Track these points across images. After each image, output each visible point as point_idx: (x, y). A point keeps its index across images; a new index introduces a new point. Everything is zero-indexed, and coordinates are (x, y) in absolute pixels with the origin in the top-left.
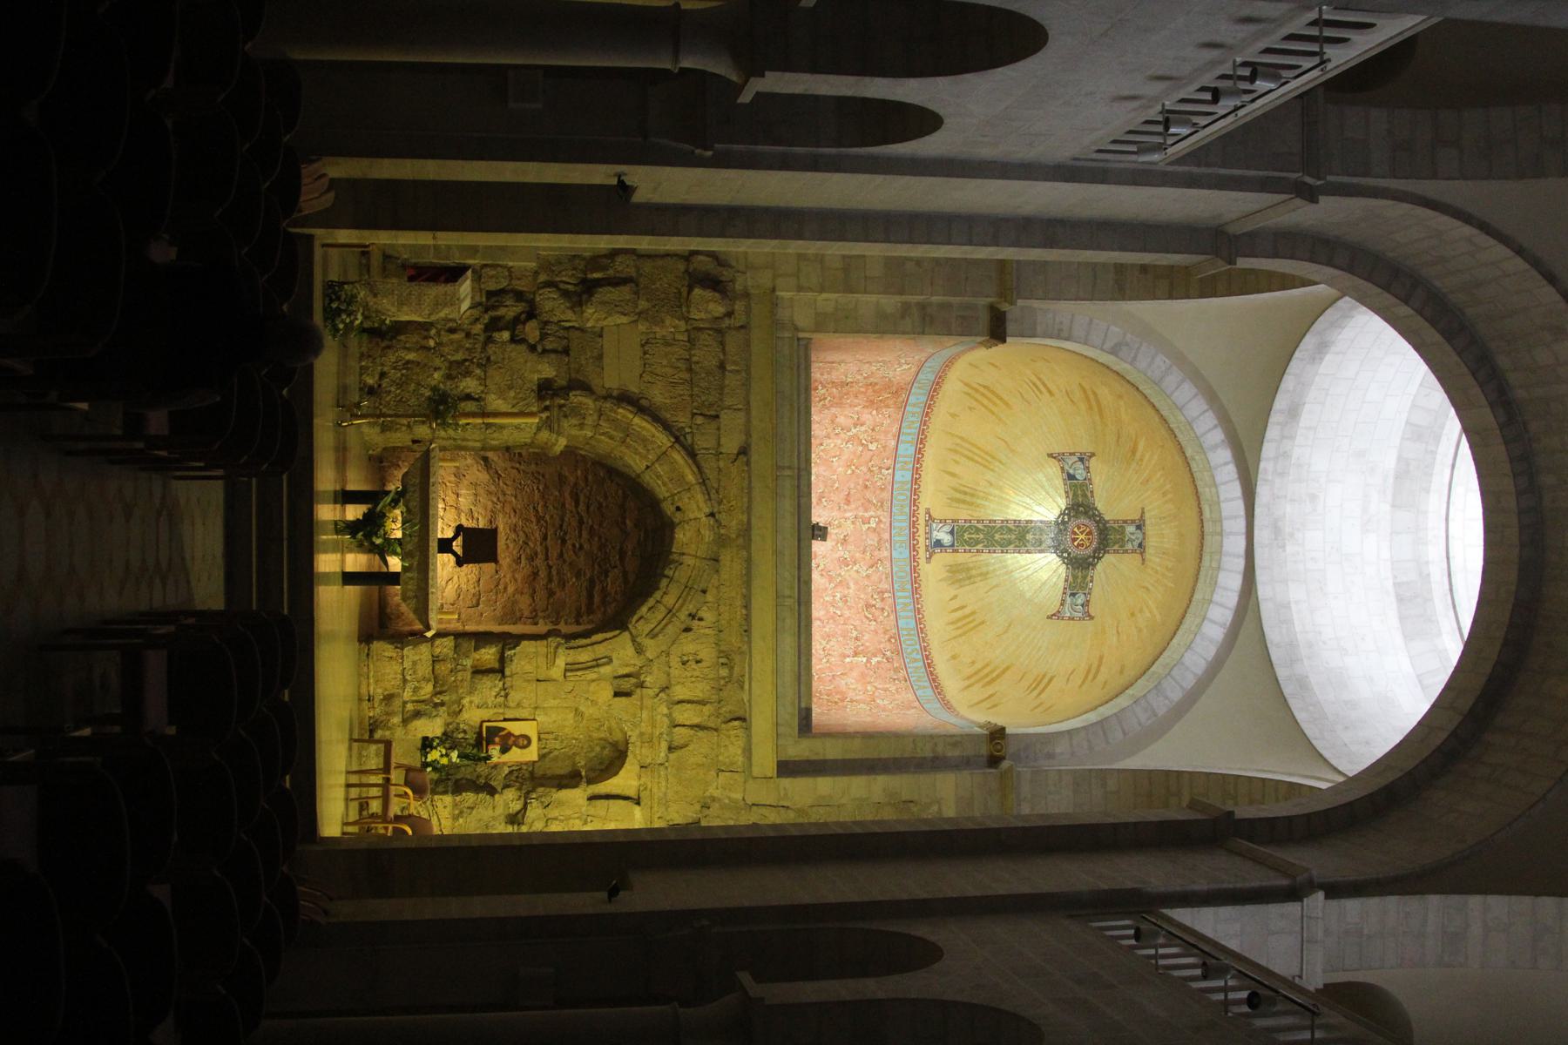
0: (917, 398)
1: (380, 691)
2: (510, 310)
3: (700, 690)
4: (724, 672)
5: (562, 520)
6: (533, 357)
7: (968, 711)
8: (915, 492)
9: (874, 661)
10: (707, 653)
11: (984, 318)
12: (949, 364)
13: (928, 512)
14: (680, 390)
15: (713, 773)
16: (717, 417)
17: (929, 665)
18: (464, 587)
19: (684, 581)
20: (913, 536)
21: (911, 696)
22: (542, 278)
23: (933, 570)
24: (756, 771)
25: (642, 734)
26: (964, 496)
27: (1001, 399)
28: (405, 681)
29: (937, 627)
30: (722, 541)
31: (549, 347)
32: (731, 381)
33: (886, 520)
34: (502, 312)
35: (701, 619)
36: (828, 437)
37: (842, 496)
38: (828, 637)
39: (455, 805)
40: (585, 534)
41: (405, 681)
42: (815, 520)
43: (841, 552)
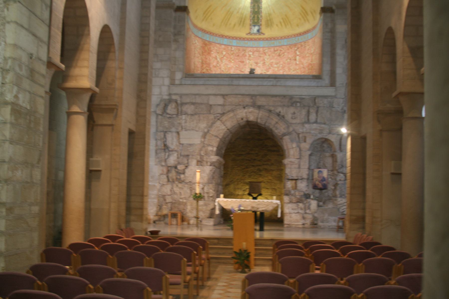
0: (207, 37)
2: (173, 174)
3: (304, 112)
7: (315, 20)
8: (240, 39)
9: (298, 53)
10: (292, 110)
11: (179, 14)
12: (195, 26)
13: (247, 34)
15: (333, 109)
16: (211, 105)
17: (300, 34)
18: (269, 193)
20: (255, 40)
21: (310, 41)
22: (163, 164)
23: (268, 33)
24: (333, 94)
25: (319, 133)
26: (242, 21)
27: (208, 8)
28: (298, 213)
29: (287, 32)
30: (254, 105)
33: (250, 49)
34: (174, 178)
35: (280, 112)
36: (220, 68)
37: (241, 64)
38: (289, 69)
39: (341, 197)
41: (298, 213)
42: (248, 73)
43: (260, 64)
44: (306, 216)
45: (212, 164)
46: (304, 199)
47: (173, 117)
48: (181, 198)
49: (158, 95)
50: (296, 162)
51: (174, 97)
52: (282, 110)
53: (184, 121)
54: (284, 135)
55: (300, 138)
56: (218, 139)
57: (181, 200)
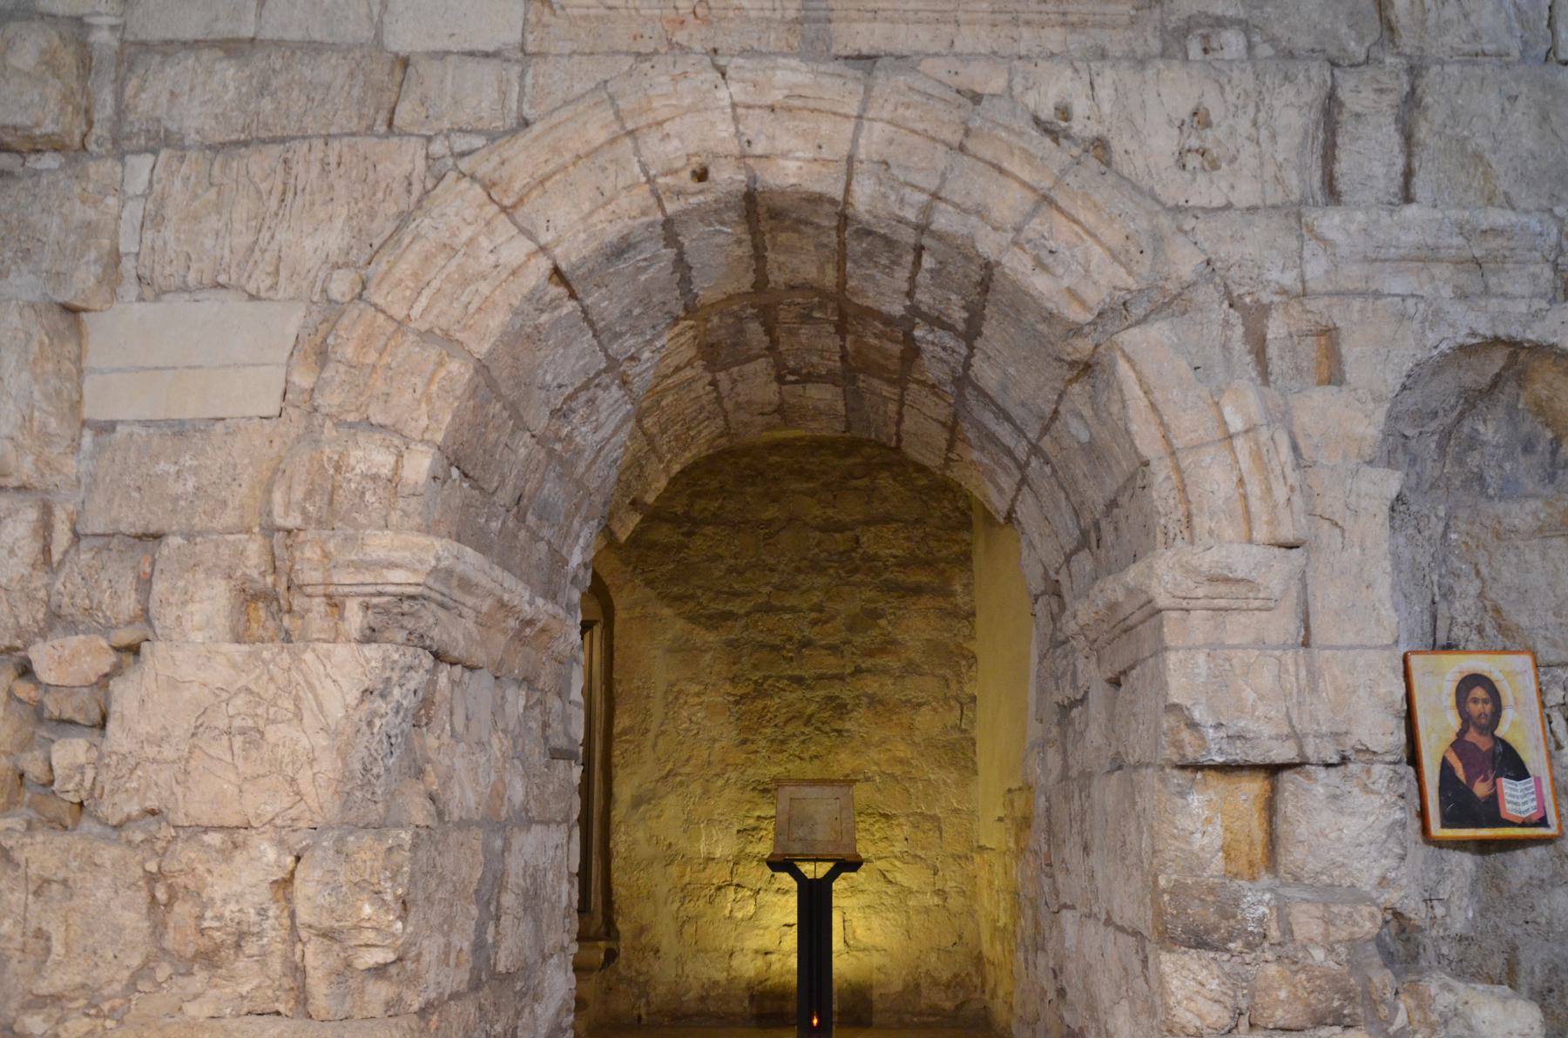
3: (1292, 111)
4: (1233, 42)
5: (762, 646)
10: (1175, 90)
14: (307, 173)
16: (405, 63)
18: (899, 847)
19: (941, 158)
25: (1462, 295)
31: (129, 604)
35: (1064, 112)
40: (790, 601)
45: (390, 617)
47: (36, 174)
53: (134, 210)
54: (1118, 312)
56: (459, 370)
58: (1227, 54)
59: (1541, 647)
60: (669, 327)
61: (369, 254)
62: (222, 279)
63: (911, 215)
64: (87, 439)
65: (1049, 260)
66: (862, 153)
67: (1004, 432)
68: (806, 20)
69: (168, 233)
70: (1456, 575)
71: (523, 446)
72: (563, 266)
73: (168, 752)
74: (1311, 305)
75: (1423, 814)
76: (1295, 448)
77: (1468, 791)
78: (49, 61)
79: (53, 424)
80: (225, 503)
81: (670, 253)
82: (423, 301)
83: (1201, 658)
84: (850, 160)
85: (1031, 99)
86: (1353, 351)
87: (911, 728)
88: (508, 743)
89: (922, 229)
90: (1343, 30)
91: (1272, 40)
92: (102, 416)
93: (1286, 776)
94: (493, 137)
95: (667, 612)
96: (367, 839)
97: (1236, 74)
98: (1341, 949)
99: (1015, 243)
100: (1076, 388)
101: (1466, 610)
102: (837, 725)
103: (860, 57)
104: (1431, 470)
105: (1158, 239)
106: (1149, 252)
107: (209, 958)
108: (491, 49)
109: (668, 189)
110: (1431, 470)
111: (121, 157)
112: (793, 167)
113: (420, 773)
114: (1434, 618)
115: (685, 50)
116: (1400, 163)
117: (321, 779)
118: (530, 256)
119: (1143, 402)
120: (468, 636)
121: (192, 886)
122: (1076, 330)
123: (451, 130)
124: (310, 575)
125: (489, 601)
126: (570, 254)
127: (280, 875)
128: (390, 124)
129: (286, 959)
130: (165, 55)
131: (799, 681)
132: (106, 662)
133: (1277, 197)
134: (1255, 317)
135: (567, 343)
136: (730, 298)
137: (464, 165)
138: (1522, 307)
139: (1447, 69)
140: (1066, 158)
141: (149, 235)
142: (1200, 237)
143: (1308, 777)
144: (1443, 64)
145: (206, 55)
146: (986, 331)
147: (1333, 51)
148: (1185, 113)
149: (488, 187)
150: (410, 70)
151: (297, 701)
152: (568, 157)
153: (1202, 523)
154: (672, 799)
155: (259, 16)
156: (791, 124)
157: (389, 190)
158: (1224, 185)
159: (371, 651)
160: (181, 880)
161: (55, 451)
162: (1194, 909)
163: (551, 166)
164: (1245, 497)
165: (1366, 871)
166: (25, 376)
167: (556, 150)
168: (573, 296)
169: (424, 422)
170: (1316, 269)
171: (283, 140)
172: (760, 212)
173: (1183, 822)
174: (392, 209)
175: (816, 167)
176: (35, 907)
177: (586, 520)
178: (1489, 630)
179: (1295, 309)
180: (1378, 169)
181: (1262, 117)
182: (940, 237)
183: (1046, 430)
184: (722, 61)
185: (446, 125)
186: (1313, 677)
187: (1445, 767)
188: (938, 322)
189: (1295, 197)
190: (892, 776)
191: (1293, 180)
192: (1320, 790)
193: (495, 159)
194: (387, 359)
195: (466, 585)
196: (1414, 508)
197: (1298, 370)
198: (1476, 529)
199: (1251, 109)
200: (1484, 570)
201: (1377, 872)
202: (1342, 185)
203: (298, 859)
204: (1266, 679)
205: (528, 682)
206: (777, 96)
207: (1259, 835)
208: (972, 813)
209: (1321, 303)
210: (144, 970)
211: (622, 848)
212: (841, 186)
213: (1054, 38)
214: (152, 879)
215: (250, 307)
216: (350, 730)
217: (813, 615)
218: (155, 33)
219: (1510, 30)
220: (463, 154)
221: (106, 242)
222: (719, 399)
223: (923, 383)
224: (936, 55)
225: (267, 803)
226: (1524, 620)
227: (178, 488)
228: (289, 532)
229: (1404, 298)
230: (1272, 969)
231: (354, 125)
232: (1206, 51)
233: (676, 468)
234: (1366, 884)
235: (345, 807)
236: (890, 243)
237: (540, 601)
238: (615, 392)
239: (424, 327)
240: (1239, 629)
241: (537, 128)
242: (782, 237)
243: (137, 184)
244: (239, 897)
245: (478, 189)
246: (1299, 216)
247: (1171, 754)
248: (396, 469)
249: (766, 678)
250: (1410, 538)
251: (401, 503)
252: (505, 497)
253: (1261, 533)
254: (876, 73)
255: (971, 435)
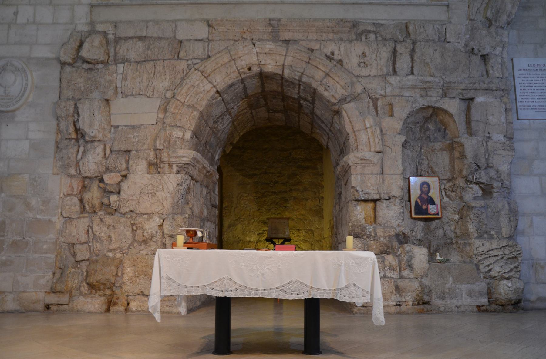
1: (393, 297)
2: (94, 194)
3: (385, 53)
4: (372, 36)
6: (131, 178)
10: (358, 48)
14: (159, 68)
15: (447, 45)
16: (181, 42)
18: (302, 238)
19: (304, 65)
22: (73, 171)
25: (421, 96)
30: (275, 37)
31: (124, 166)
32: (153, 32)
34: (96, 203)
35: (333, 53)
39: (480, 237)
44: (401, 283)
45: (182, 168)
46: (396, 244)
47: (98, 69)
48: (110, 250)
49: (66, 24)
50: (375, 160)
51: (100, 28)
52: (339, 50)
53: (120, 77)
54: (344, 100)
55: (378, 106)
56: (196, 114)
57: (110, 254)
58: (371, 39)
59: (440, 176)
60: (241, 101)
61: (176, 86)
62: (141, 93)
63: (297, 78)
64: (112, 130)
65: (328, 88)
66: (286, 64)
67: (323, 125)
68: (274, 32)
69: (128, 82)
70: (423, 159)
71: (208, 130)
72: (219, 90)
73: (135, 198)
74: (387, 98)
75: (411, 212)
76: (381, 131)
77: (421, 207)
78: (101, 43)
79: (106, 126)
80: (145, 144)
81: (242, 86)
82: (188, 98)
83: (359, 176)
84: (283, 65)
85: (325, 51)
86: (396, 109)
87: (305, 206)
88: (204, 200)
89: (300, 81)
90: (398, 34)
91: (382, 36)
92: (116, 124)
93: (378, 202)
94: (202, 60)
95: (238, 174)
96: (179, 216)
97: (372, 44)
98: (387, 238)
99: (320, 84)
100: (336, 117)
101: (425, 167)
102: (285, 205)
103: (286, 41)
104: (418, 135)
105: (352, 84)
106: (350, 87)
107: (145, 242)
108: (201, 39)
109: (243, 72)
110: (418, 135)
111: (116, 64)
112: (270, 67)
113: (188, 203)
114: (417, 169)
115: (246, 39)
116: (410, 65)
117: (168, 204)
118: (211, 88)
119: (348, 121)
120: (197, 174)
121: (141, 226)
122: (334, 104)
123: (192, 58)
124: (165, 159)
125: (201, 166)
126: (220, 87)
127: (160, 224)
128: (178, 56)
129: (161, 242)
130: (125, 40)
131: (274, 193)
132: (120, 179)
133: (381, 74)
134: (375, 101)
135: (218, 106)
136: (256, 94)
137: (196, 66)
138: (435, 99)
139: (421, 43)
140: (332, 65)
141: (124, 83)
142: (363, 83)
143: (382, 202)
144: (420, 42)
145: (135, 40)
146: (316, 102)
147: (395, 39)
148: (360, 54)
149: (202, 72)
150: (182, 44)
151: (163, 187)
152: (220, 65)
153: (360, 147)
154: (239, 225)
155: (146, 31)
156: (270, 57)
157: (178, 72)
158: (369, 71)
159: (179, 176)
160: (139, 225)
161: (106, 132)
162: (356, 229)
163: (216, 67)
164: (369, 141)
165: (395, 223)
166: (100, 116)
167: (217, 64)
168: (220, 96)
169: (189, 125)
170: (389, 90)
171: (153, 60)
172: (263, 76)
173: (356, 212)
174: (179, 77)
175: (276, 67)
176: (108, 231)
177: (219, 148)
178: (430, 172)
179: (384, 99)
180: (405, 66)
181: (378, 54)
182: (304, 83)
183: (331, 126)
184: (254, 42)
185: (191, 57)
186: (383, 181)
187: (416, 202)
188: (306, 100)
189: (385, 73)
190: (300, 219)
191: (384, 69)
192: (384, 205)
193: (203, 66)
194: (180, 111)
195: (198, 162)
196: (412, 144)
197: (385, 113)
198: (428, 149)
199: (376, 52)
200: (429, 159)
201: (397, 223)
202: (397, 70)
203: (164, 221)
204: (373, 181)
205: (207, 187)
206: (267, 51)
207: (372, 216)
208: (322, 229)
209: (390, 98)
210: (132, 244)
211: (226, 239)
212: (281, 71)
213: (331, 36)
214: (132, 225)
215: (148, 99)
216: (174, 193)
217: (278, 175)
218: (123, 35)
219: (436, 34)
220: (195, 64)
221: (114, 85)
222: (253, 117)
223: (304, 113)
224: (303, 40)
225: (157, 208)
226: (437, 170)
227: (134, 140)
228: (160, 150)
229: (408, 97)
230: (372, 242)
231: (170, 57)
232: (366, 38)
233: (242, 134)
234: (395, 225)
235: (173, 210)
236: (293, 83)
237: (211, 167)
238: (228, 116)
239: (188, 104)
240: (367, 170)
241: (213, 59)
242: (268, 81)
243: (120, 70)
244: (151, 228)
245: (200, 73)
246: (385, 78)
247: (353, 197)
248: (183, 136)
249: (265, 192)
250: (412, 151)
251: (184, 143)
252: (203, 142)
253: (373, 150)
254: (289, 45)
255: (316, 126)
